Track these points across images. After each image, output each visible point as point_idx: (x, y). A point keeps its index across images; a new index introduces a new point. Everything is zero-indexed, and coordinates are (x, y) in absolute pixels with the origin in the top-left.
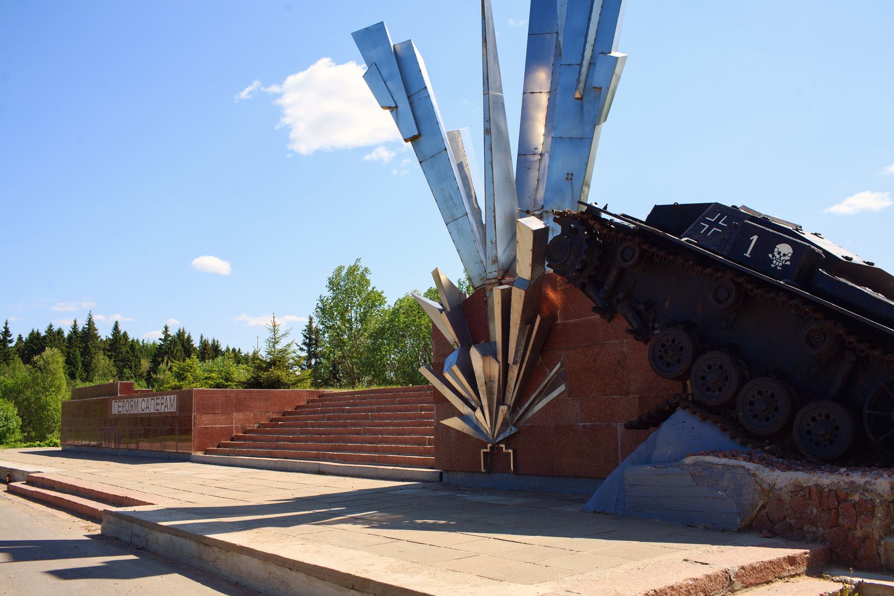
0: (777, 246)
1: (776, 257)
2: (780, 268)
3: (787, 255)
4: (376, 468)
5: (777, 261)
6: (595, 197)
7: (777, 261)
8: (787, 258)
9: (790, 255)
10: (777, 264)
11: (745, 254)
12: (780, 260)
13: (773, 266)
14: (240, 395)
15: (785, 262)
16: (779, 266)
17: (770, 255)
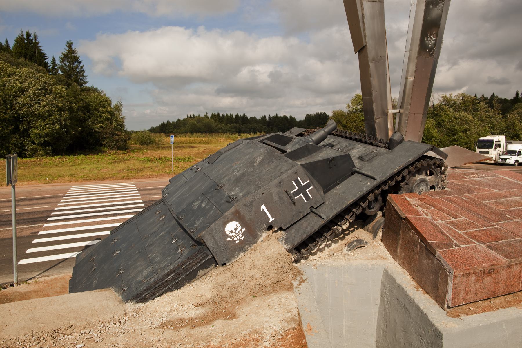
0: (225, 231)
1: (233, 236)
2: (243, 237)
3: (237, 227)
5: (236, 237)
7: (236, 237)
8: (239, 229)
9: (239, 225)
10: (238, 238)
11: (270, 221)
12: (237, 234)
13: (237, 242)
15: (241, 231)
16: (242, 237)
17: (228, 239)
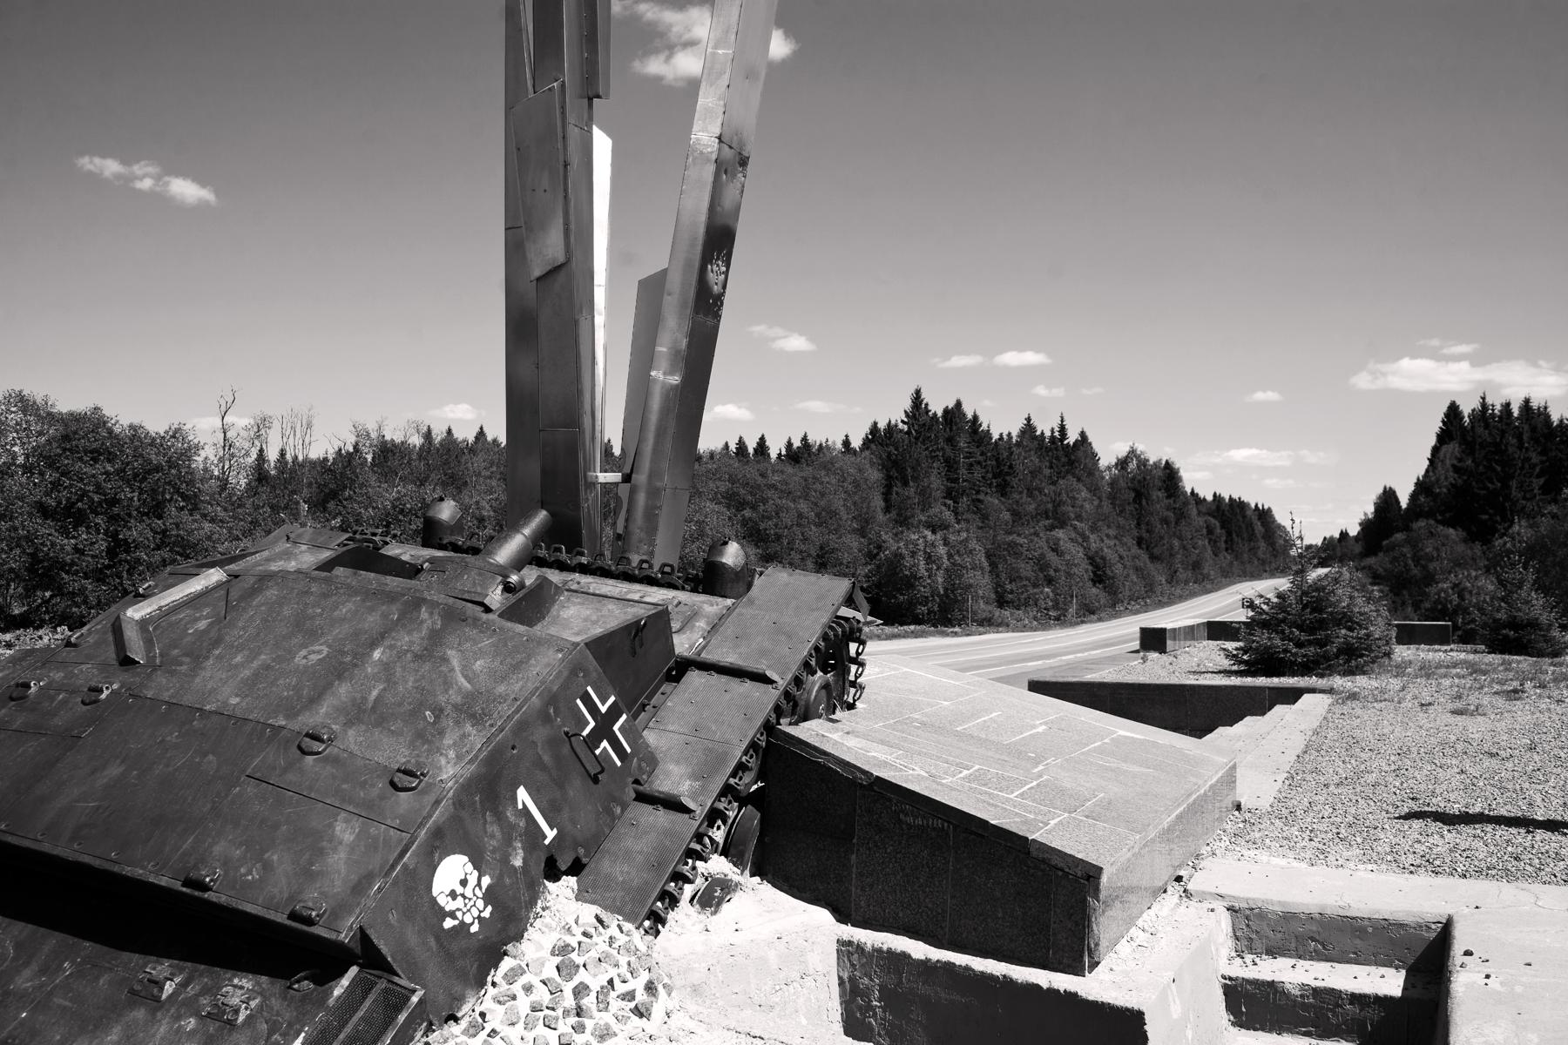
1: (458, 909)
4: (1134, 732)
6: (575, 878)
8: (473, 880)
9: (470, 867)
11: (547, 842)
13: (475, 928)
14: (1120, 694)
15: (481, 889)
